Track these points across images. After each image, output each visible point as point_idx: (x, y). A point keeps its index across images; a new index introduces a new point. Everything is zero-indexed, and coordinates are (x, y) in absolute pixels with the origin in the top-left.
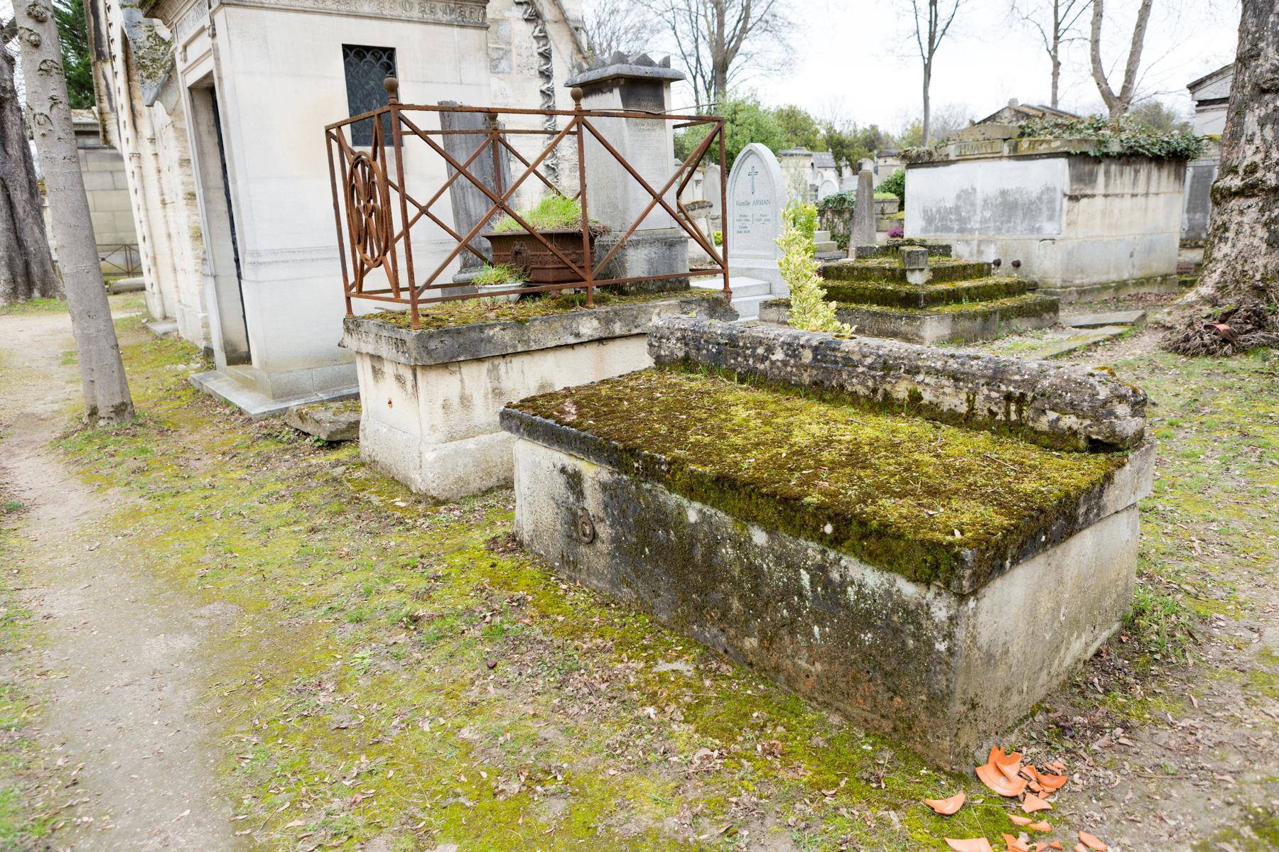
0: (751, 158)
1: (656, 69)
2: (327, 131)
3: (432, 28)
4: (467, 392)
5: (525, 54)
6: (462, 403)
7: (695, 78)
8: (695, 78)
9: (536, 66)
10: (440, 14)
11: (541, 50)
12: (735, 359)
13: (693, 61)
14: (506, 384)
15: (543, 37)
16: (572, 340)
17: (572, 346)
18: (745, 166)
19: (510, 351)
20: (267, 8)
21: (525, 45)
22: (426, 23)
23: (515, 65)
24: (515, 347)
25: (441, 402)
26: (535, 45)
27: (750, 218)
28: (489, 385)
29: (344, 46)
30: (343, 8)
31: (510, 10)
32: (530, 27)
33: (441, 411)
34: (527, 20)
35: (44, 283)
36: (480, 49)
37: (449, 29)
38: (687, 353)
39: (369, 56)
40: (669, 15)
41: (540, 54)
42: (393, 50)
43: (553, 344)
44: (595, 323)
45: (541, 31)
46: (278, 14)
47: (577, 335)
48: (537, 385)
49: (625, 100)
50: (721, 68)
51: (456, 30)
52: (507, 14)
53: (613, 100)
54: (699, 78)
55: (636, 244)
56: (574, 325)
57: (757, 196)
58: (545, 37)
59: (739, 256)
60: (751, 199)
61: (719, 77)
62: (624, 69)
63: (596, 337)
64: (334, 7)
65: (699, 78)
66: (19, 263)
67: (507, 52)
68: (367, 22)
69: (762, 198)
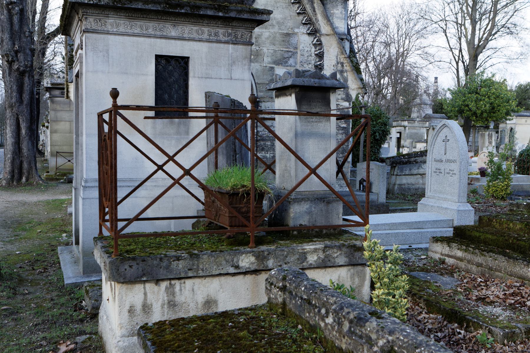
0: (445, 130)
1: (328, 82)
2: (100, 115)
3: (215, 45)
4: (149, 302)
5: (306, 54)
6: (144, 309)
7: (457, 63)
8: (457, 63)
9: (313, 62)
10: (221, 36)
11: (316, 53)
12: (309, 314)
13: (457, 52)
14: (179, 298)
15: (319, 44)
16: (232, 270)
17: (234, 275)
18: (441, 134)
19: (183, 275)
20: (111, 34)
21: (306, 49)
22: (212, 42)
23: (299, 62)
24: (186, 273)
25: (127, 307)
26: (313, 49)
27: (442, 171)
28: (166, 298)
29: (156, 56)
30: (158, 33)
31: (298, 28)
32: (311, 38)
33: (127, 314)
34: (309, 34)
35: (29, 174)
36: (246, 58)
37: (226, 45)
38: (284, 300)
39: (173, 62)
40: (442, 24)
41: (316, 55)
42: (188, 58)
43: (217, 273)
44: (253, 259)
45: (317, 41)
46: (117, 37)
47: (237, 267)
48: (203, 300)
49: (298, 101)
50: (474, 58)
51: (231, 46)
52: (296, 30)
53: (289, 102)
54: (460, 64)
55: (298, 200)
56: (235, 260)
57: (449, 156)
58: (321, 44)
59: (433, 198)
60: (444, 158)
61: (473, 63)
62: (300, 81)
63: (252, 269)
64: (153, 33)
65: (460, 64)
66: (18, 161)
67: (294, 54)
68: (173, 41)
69: (451, 158)
